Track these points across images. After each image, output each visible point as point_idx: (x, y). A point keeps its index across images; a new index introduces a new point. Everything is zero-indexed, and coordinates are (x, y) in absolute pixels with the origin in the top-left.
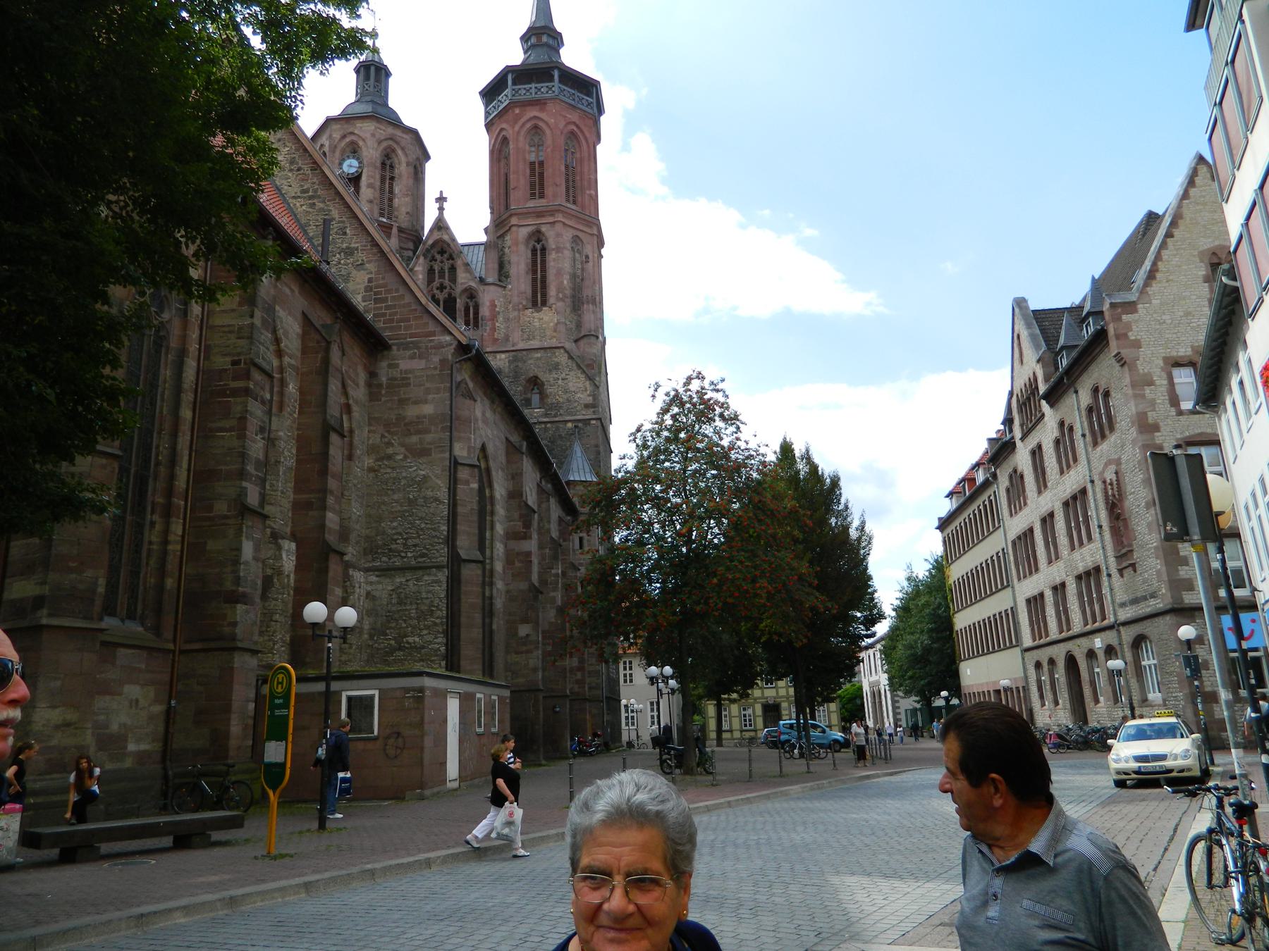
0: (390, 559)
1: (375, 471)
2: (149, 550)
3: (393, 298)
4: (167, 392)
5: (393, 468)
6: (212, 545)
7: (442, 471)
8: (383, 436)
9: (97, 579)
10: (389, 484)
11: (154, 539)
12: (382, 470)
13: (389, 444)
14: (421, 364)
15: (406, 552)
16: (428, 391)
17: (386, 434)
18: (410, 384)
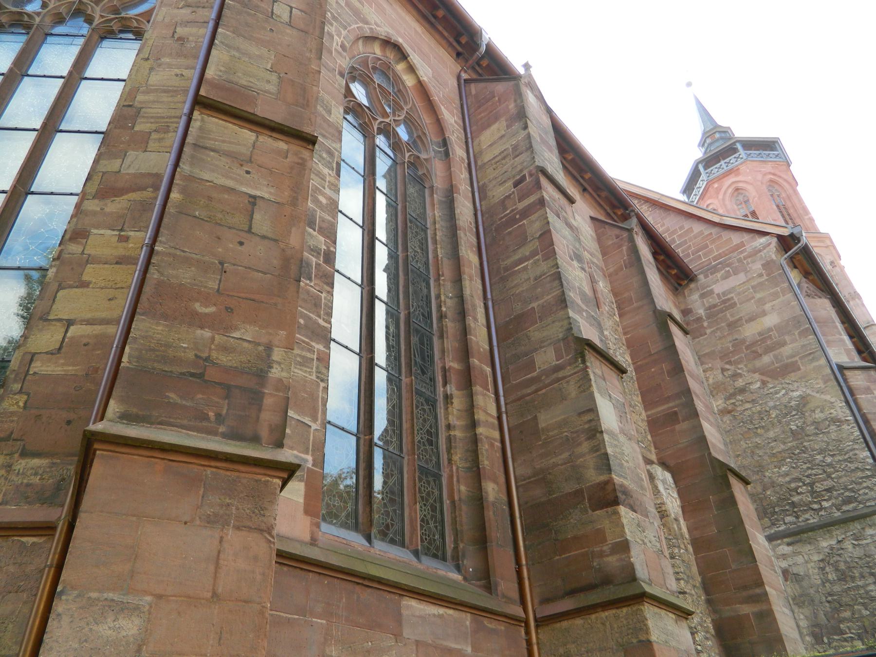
0: (797, 517)
1: (729, 412)
2: (449, 439)
3: (680, 236)
4: (439, 234)
5: (753, 401)
6: (545, 419)
7: (825, 383)
8: (723, 370)
9: (269, 348)
10: (755, 422)
11: (453, 420)
12: (739, 409)
13: (735, 376)
14: (742, 277)
15: (819, 503)
16: (761, 302)
17: (728, 367)
18: (735, 304)
